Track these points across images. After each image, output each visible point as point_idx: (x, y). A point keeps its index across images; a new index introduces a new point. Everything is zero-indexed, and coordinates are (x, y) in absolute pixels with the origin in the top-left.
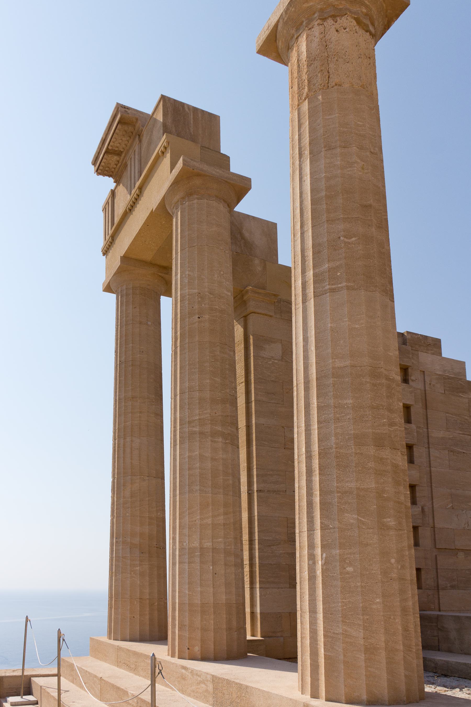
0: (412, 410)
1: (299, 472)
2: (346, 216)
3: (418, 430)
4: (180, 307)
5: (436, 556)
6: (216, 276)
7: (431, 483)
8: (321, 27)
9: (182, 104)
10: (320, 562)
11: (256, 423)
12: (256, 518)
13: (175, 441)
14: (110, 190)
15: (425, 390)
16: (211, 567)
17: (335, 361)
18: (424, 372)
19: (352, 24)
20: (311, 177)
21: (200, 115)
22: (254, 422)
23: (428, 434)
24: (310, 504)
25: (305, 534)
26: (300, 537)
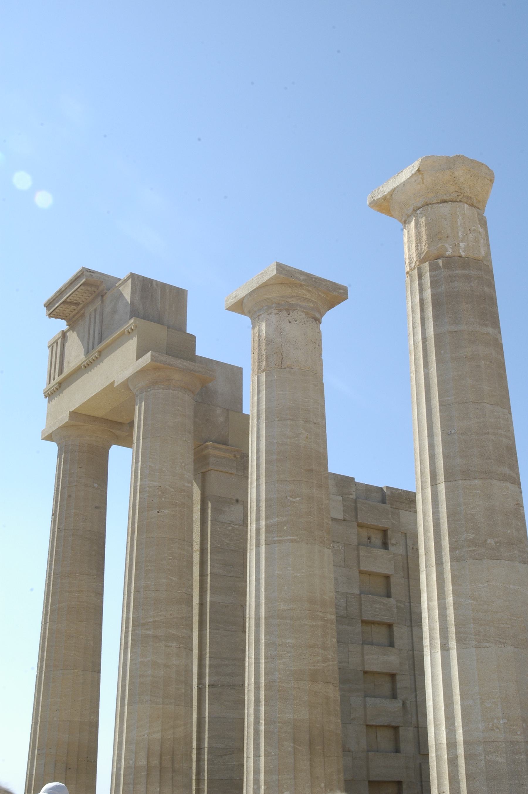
0: (392, 580)
1: (248, 700)
2: (293, 479)
3: (399, 604)
4: (139, 498)
5: (420, 764)
6: (177, 469)
7: (414, 670)
8: (277, 316)
9: (151, 281)
10: (263, 787)
11: (210, 601)
12: (207, 719)
13: (126, 643)
14: (60, 330)
15: (407, 556)
16: (158, 789)
17: (280, 604)
18: (406, 534)
19: (302, 317)
20: (266, 440)
21: (168, 291)
22: (208, 600)
23: (410, 609)
24: (257, 732)
25: (251, 760)
26: (247, 762)
